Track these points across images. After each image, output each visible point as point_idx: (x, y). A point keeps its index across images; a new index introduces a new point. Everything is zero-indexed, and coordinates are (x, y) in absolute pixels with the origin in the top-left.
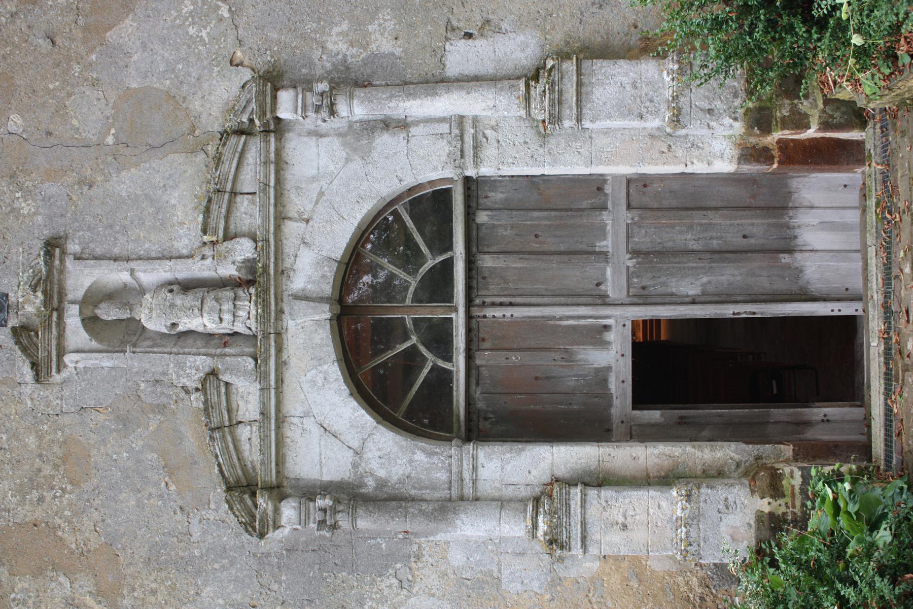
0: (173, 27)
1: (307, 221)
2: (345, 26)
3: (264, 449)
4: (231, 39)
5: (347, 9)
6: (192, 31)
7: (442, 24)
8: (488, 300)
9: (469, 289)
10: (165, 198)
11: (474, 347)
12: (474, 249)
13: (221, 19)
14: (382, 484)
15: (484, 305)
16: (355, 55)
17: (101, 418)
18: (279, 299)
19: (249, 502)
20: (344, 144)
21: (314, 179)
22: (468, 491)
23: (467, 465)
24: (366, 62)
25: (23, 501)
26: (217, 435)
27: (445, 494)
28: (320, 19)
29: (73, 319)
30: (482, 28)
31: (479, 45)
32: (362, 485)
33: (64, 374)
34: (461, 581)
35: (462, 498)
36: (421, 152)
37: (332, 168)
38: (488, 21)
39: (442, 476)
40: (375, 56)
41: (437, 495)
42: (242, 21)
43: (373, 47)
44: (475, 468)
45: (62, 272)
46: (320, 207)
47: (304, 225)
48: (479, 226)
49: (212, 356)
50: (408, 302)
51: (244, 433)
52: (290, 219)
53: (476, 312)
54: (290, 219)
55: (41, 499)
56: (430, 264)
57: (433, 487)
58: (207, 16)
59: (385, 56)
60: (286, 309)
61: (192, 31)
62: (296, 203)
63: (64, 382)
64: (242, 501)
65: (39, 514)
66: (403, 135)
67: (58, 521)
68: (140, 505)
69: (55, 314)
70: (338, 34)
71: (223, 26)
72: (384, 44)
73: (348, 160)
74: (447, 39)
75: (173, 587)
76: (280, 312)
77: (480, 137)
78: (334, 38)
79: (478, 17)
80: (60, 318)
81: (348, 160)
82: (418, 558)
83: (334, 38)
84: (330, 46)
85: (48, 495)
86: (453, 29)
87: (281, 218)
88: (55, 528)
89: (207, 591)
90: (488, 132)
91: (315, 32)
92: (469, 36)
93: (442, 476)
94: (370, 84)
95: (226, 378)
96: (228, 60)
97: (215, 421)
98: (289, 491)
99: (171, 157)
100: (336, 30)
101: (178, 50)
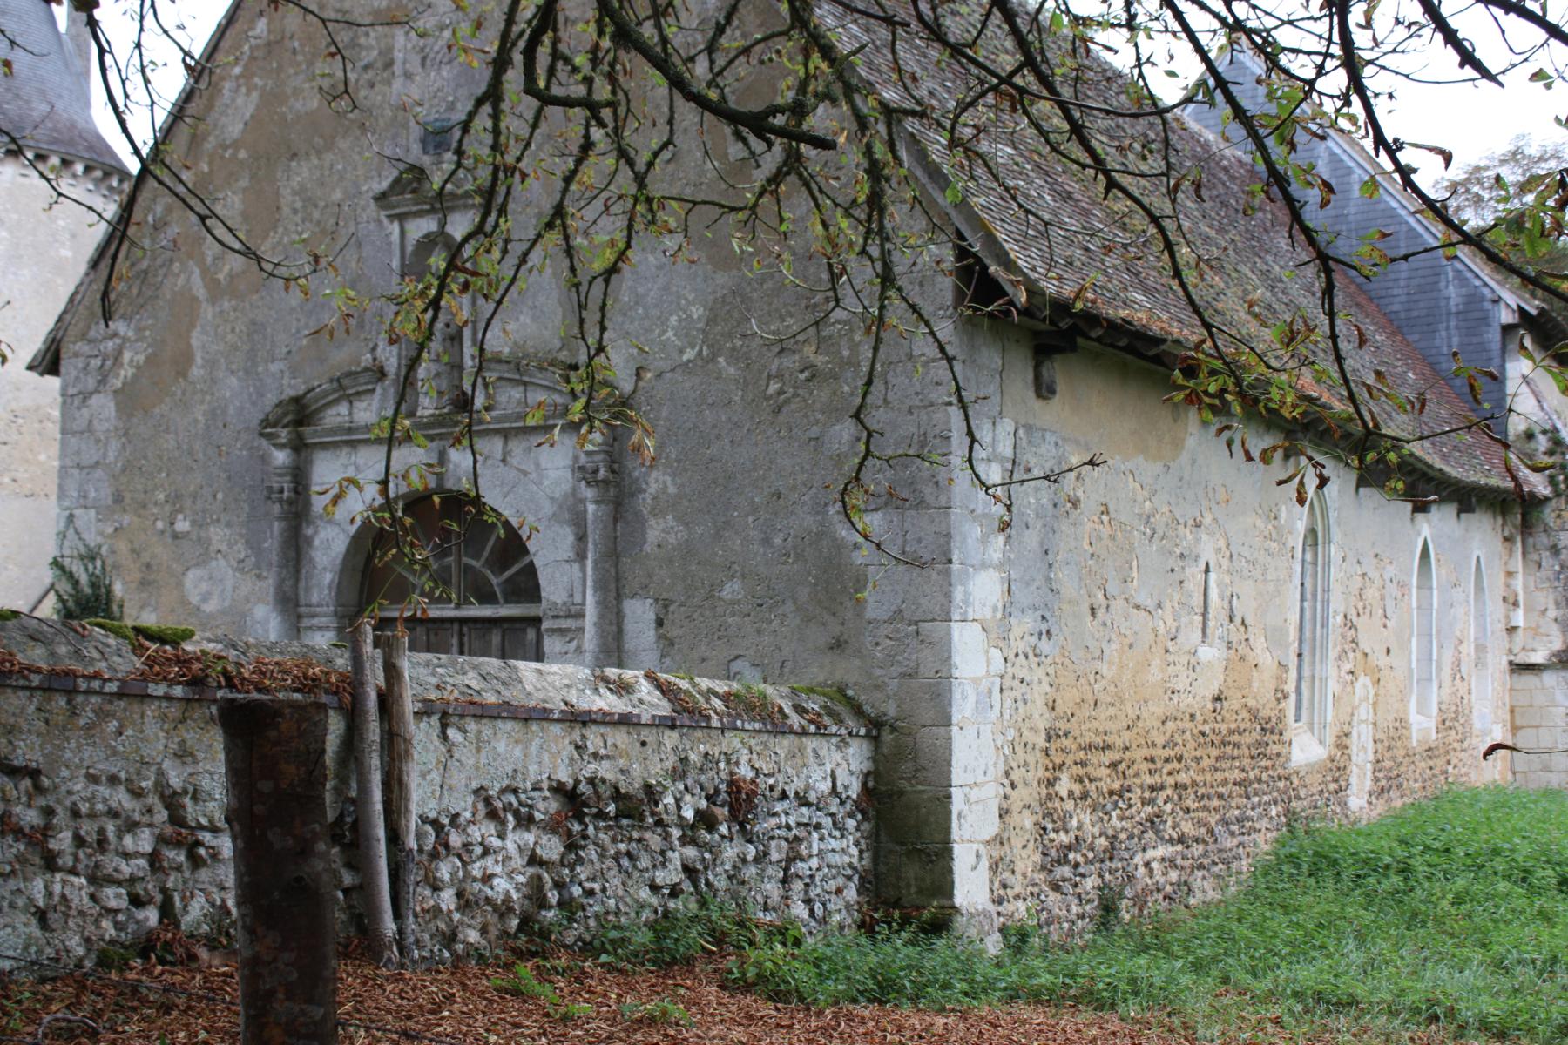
0: (679, 297)
1: (504, 461)
2: (672, 490)
3: (333, 431)
4: (662, 365)
5: (687, 490)
6: (673, 320)
7: (671, 595)
8: (466, 639)
9: (475, 620)
10: (525, 310)
11: (430, 625)
12: (506, 626)
13: (681, 351)
14: (309, 542)
15: (461, 635)
16: (645, 502)
17: (353, 265)
18: (441, 436)
19: (286, 421)
20: (566, 495)
21: (537, 465)
22: (306, 622)
23: (322, 621)
24: (638, 514)
25: (295, 193)
26: (335, 385)
27: (302, 601)
28: (679, 461)
29: (428, 225)
30: (666, 638)
31: (650, 635)
32: (309, 523)
33: (386, 221)
34: (243, 616)
35: (299, 617)
36: (557, 575)
37: (546, 483)
38: (672, 644)
39: (315, 599)
40: (642, 522)
41: (302, 593)
42: (678, 376)
43: (652, 522)
44: (320, 629)
45: (466, 207)
46: (514, 473)
47: (499, 456)
48: (524, 631)
49: (398, 375)
50: (465, 560)
51: (343, 409)
52: (506, 443)
53: (456, 627)
54: (506, 443)
55: (295, 211)
56: (494, 581)
57: (308, 590)
58: (687, 335)
59: (644, 534)
60: (434, 444)
61: (673, 320)
62: (517, 446)
63: (379, 222)
64: (285, 414)
65: (286, 211)
66: (572, 555)
67: (280, 230)
68: (293, 310)
69: (427, 207)
70: (665, 483)
71: (675, 355)
72: (655, 531)
73: (552, 499)
74: (657, 600)
75: (236, 348)
76: (431, 438)
77: (570, 635)
78: (661, 478)
79: (675, 633)
80: (428, 212)
81: (552, 499)
82: (259, 577)
83: (661, 478)
84: (654, 474)
85: (298, 218)
86: (666, 607)
87: (506, 434)
88: (275, 228)
89: (233, 381)
90: (574, 643)
91: (667, 458)
92: (660, 623)
93: (315, 599)
94: (616, 521)
95: (379, 390)
96: (643, 363)
97: (345, 382)
98: (303, 454)
99: (560, 311)
100: (668, 479)
101: (656, 306)
